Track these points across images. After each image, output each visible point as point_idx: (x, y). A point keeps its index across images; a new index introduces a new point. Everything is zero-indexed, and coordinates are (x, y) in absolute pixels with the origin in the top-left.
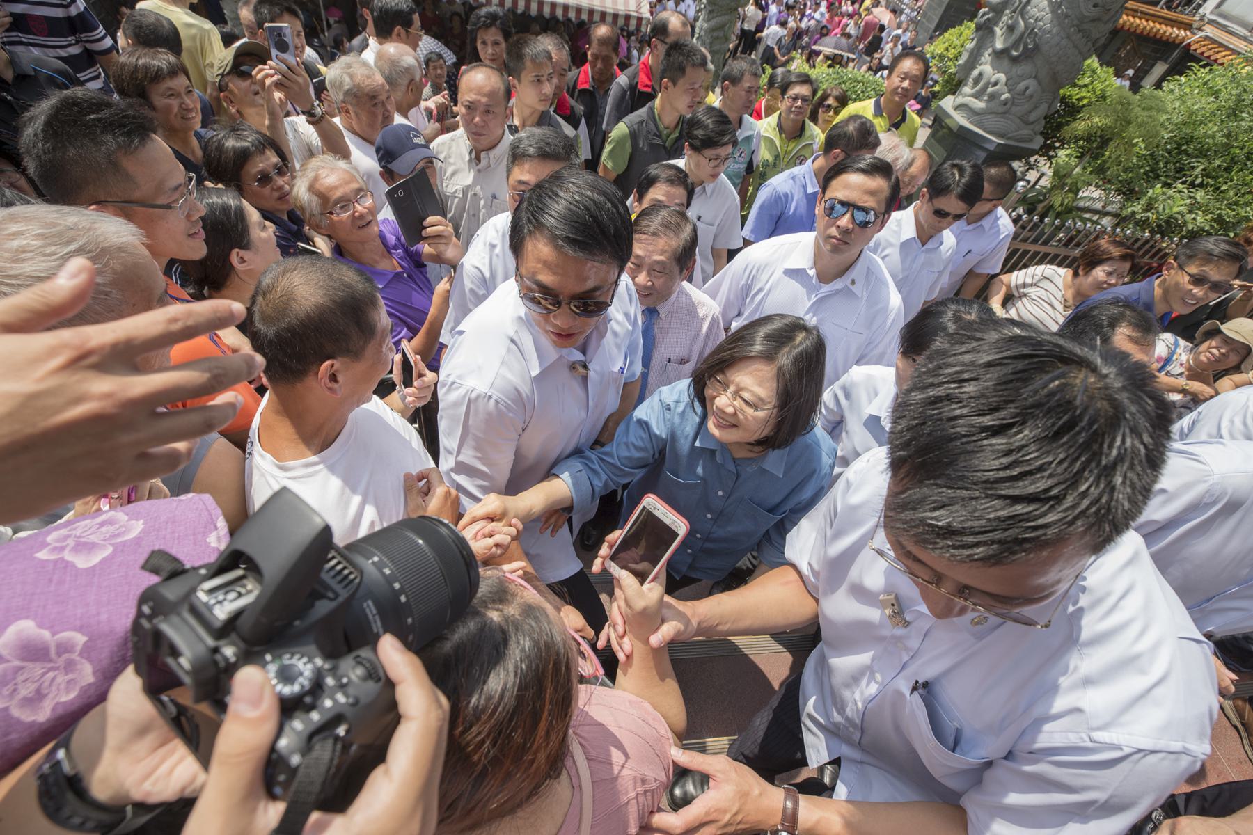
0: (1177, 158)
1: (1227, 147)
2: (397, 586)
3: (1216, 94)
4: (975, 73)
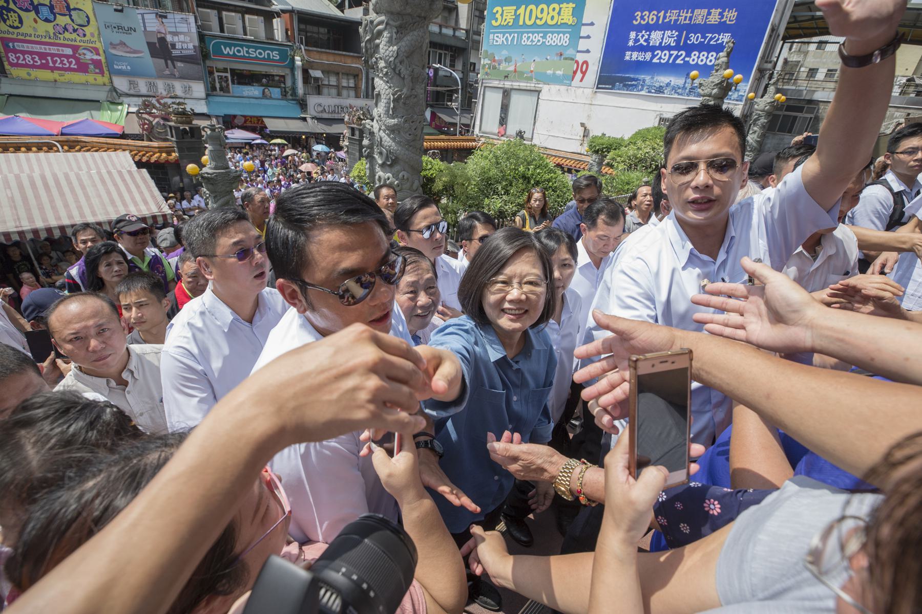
0: (488, 186)
1: (504, 176)
2: (365, 586)
3: (486, 158)
4: (377, 177)
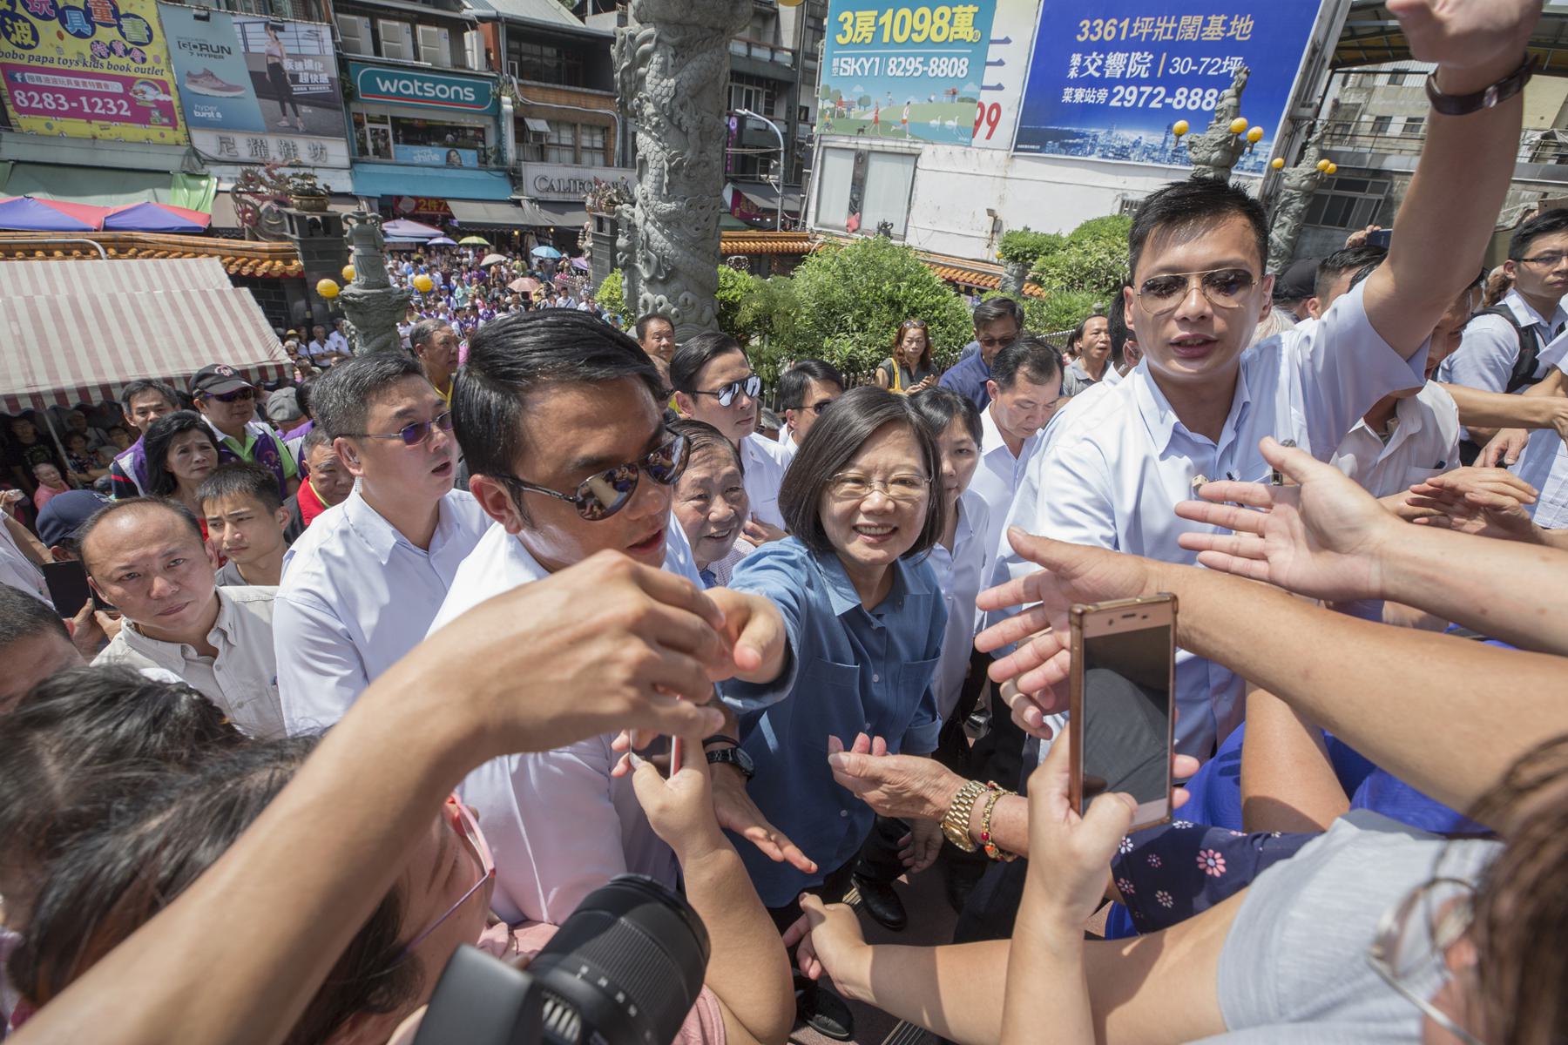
0: (830, 316)
1: (856, 300)
3: (827, 268)
4: (641, 301)
